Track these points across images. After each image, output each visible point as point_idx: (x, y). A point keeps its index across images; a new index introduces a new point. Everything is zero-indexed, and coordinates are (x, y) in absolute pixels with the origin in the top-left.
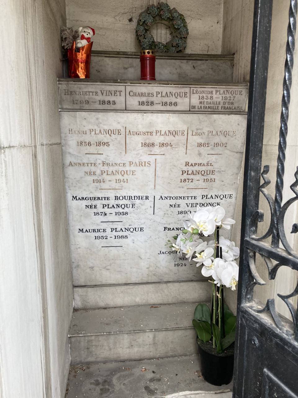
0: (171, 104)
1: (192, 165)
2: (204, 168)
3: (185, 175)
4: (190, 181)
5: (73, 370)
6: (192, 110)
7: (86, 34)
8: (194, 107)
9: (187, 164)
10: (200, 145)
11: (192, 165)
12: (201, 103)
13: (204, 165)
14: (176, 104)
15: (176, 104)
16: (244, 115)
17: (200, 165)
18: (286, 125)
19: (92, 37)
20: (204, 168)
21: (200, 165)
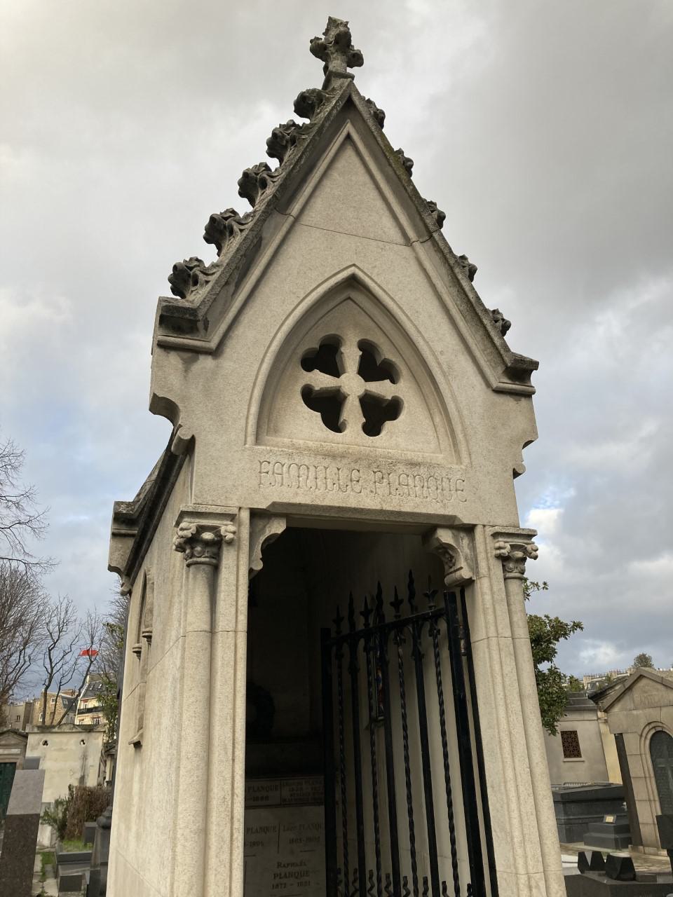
0: (262, 798)
1: (284, 866)
2: (297, 869)
3: (277, 878)
4: (283, 886)
5: (222, 866)
6: (283, 804)
7: (81, 739)
8: (285, 800)
9: (279, 865)
10: (292, 841)
11: (284, 866)
12: (291, 795)
13: (297, 865)
14: (267, 798)
15: (267, 798)
16: (340, 164)
17: (293, 865)
18: (347, 868)
19: (513, 482)
20: (297, 869)
21: (293, 865)
